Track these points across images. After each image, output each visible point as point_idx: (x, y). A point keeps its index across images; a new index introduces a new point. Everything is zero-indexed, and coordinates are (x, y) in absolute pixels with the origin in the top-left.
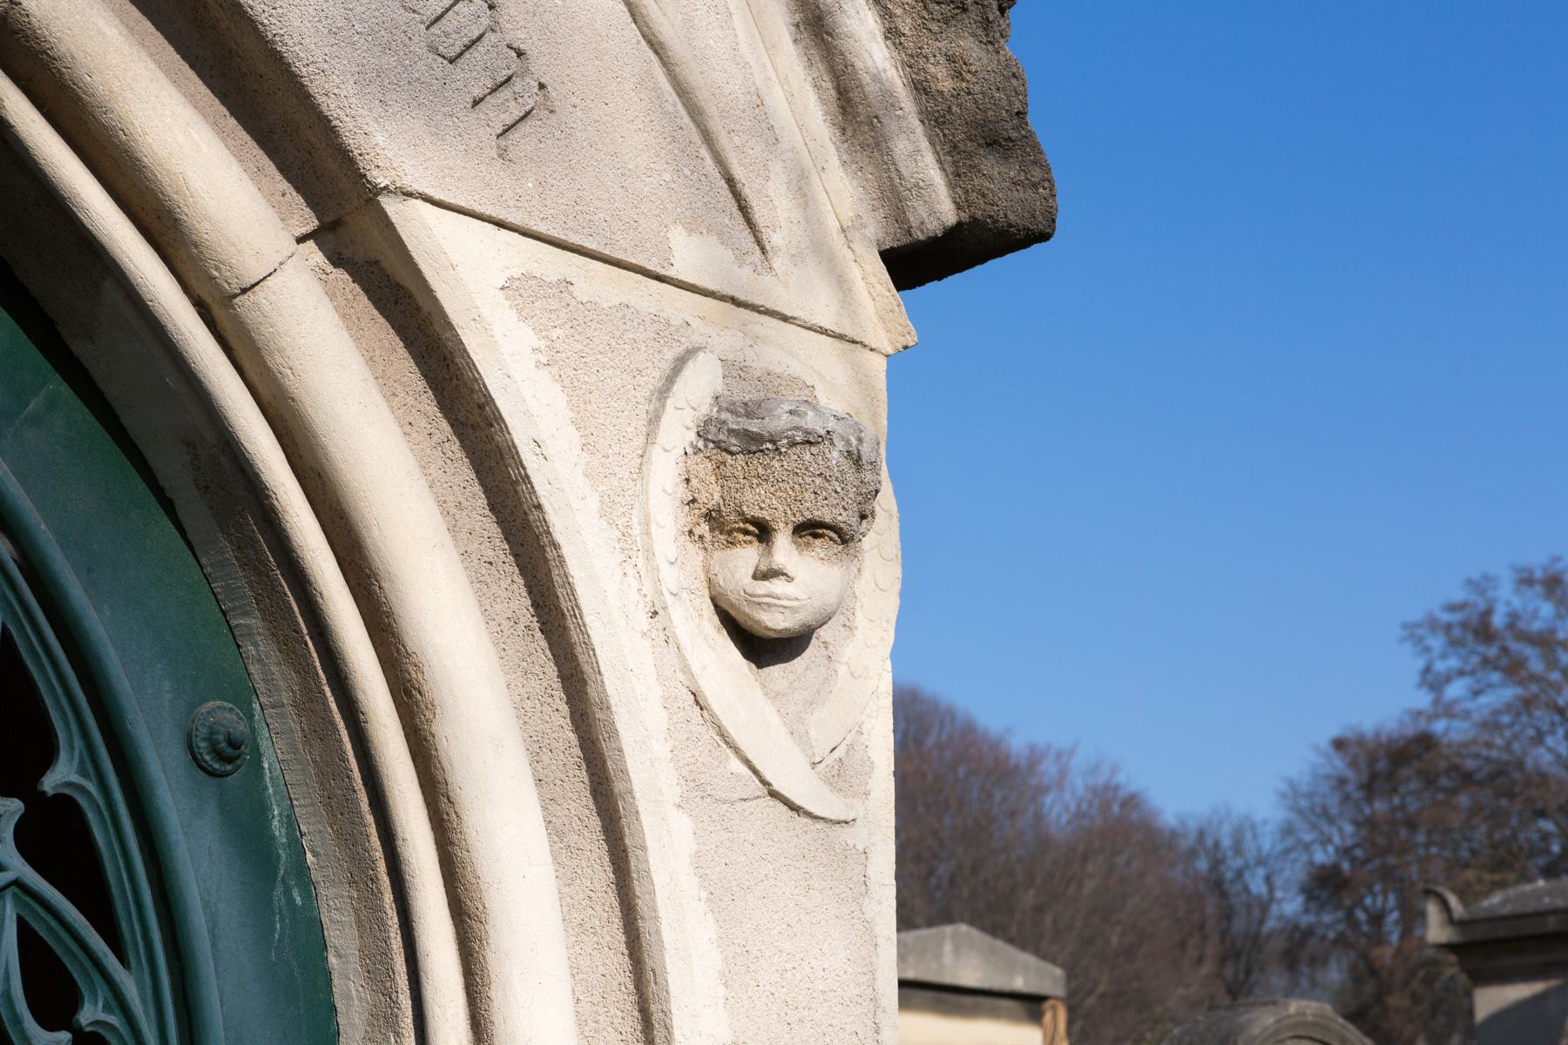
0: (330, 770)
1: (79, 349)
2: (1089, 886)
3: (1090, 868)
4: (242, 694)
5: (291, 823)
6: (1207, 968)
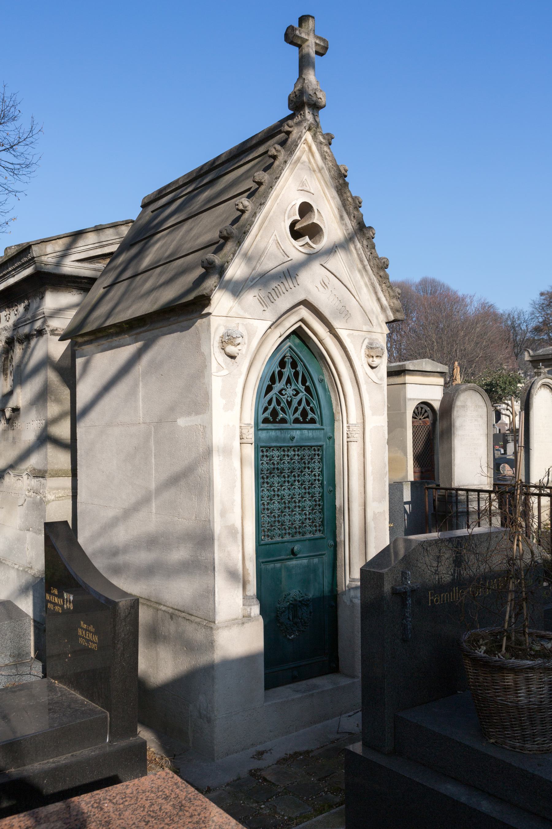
0: (331, 382)
1: (308, 344)
2: (478, 329)
3: (478, 326)
4: (323, 375)
5: (328, 386)
6: (509, 350)
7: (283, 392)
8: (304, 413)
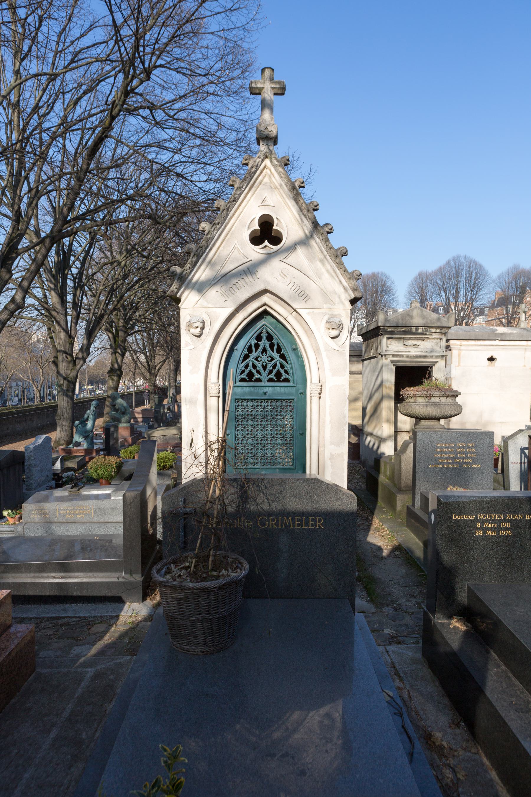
7: (259, 359)
8: (278, 375)
